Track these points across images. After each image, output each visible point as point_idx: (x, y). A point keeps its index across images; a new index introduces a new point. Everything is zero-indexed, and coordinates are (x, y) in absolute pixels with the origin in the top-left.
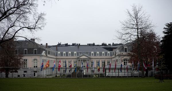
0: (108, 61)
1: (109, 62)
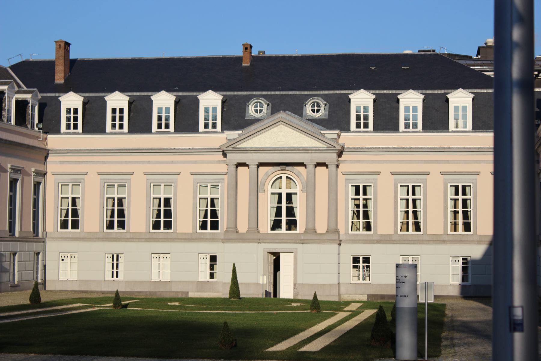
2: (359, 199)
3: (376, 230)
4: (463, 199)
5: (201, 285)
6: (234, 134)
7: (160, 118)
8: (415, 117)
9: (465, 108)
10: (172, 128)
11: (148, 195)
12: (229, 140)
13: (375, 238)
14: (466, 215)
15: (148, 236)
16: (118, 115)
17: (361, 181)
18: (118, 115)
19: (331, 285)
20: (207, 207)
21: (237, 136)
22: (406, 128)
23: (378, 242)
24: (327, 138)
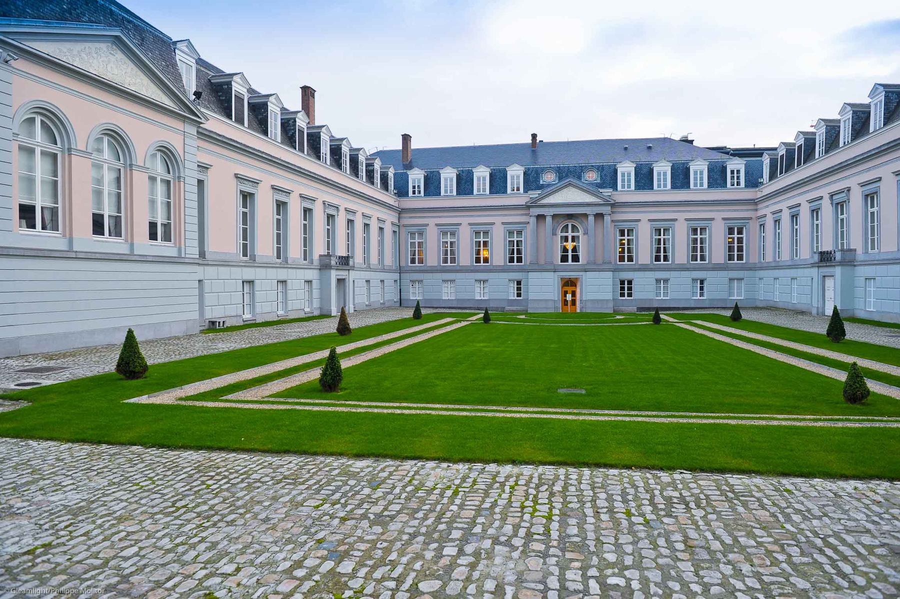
0: (731, 223)
1: (736, 224)
2: (624, 240)
3: (673, 261)
4: (738, 238)
5: (511, 302)
6: (534, 194)
7: (414, 187)
8: (518, 183)
9: (451, 180)
10: (743, 184)
11: (439, 240)
12: (531, 198)
13: (637, 267)
14: (452, 252)
15: (472, 268)
16: (735, 175)
17: (626, 226)
18: (735, 175)
19: (607, 300)
20: (514, 246)
21: (538, 195)
22: (460, 192)
23: (639, 270)
24: (604, 196)
